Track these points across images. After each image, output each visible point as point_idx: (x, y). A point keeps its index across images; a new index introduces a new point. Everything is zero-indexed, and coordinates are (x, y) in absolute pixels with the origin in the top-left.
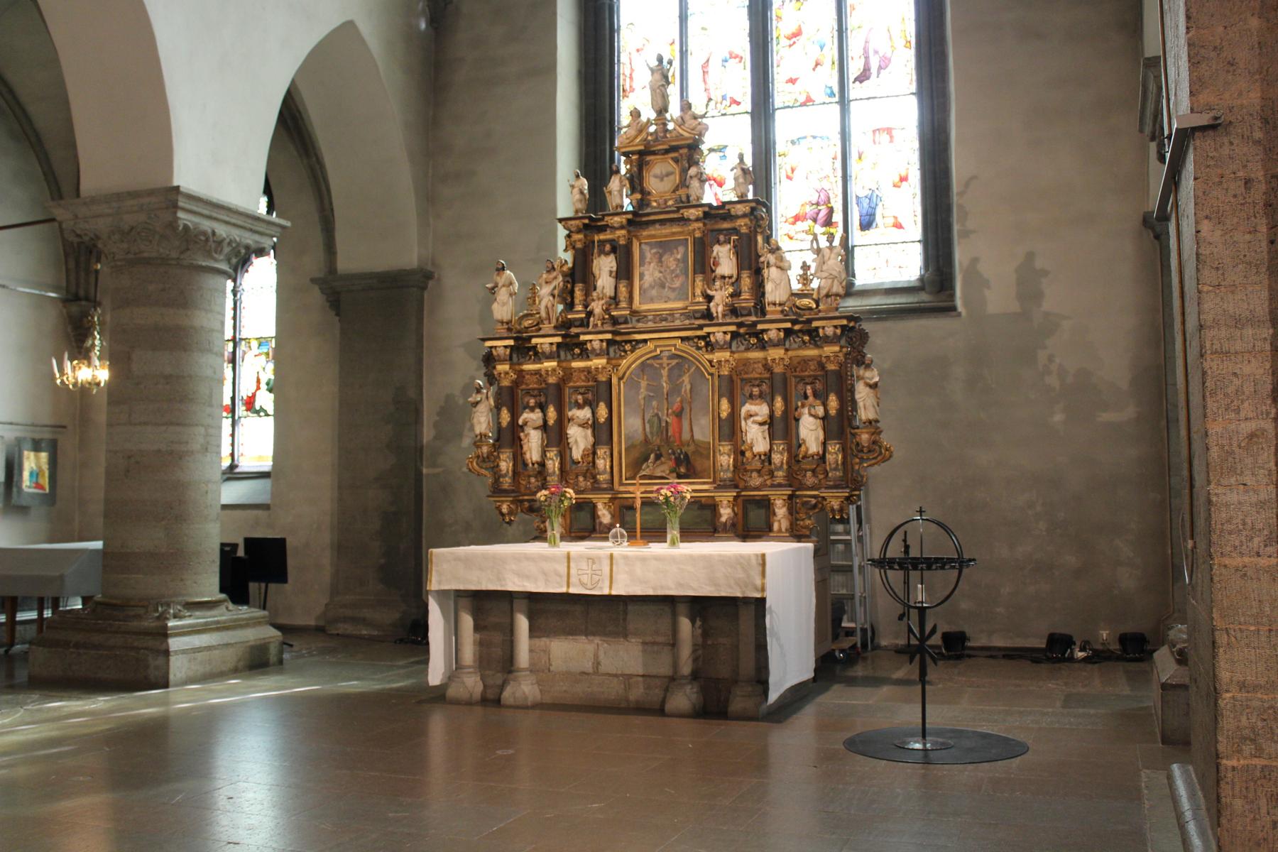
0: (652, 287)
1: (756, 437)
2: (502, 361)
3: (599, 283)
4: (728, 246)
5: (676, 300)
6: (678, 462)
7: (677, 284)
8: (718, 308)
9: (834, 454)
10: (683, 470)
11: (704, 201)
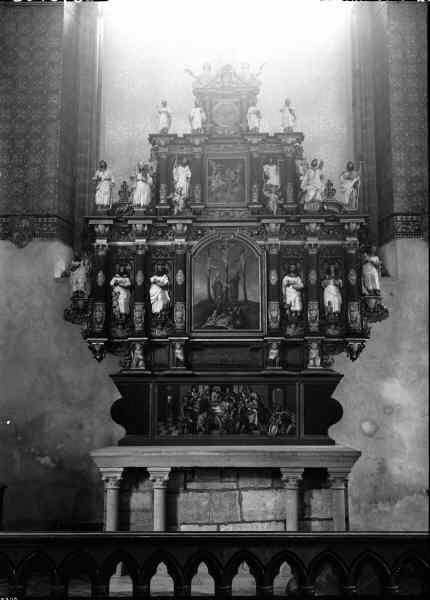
0: (217, 191)
1: (292, 297)
2: (102, 237)
3: (178, 186)
4: (275, 167)
5: (119, 247)
6: (235, 317)
7: (236, 190)
8: (273, 206)
9: (355, 313)
10: (238, 322)
11: (261, 131)
